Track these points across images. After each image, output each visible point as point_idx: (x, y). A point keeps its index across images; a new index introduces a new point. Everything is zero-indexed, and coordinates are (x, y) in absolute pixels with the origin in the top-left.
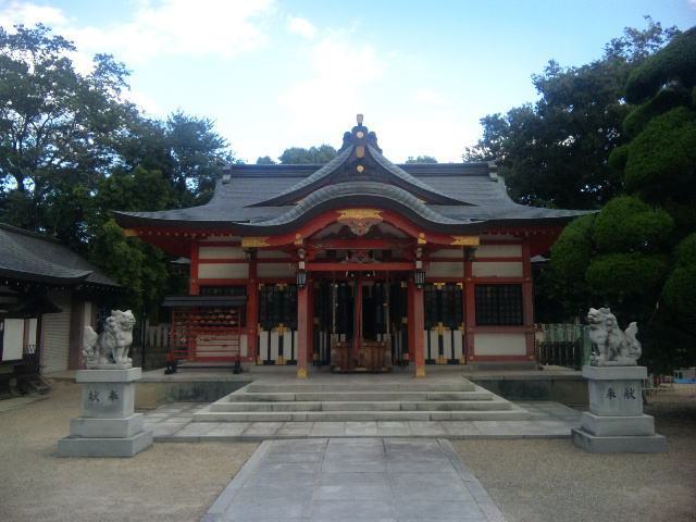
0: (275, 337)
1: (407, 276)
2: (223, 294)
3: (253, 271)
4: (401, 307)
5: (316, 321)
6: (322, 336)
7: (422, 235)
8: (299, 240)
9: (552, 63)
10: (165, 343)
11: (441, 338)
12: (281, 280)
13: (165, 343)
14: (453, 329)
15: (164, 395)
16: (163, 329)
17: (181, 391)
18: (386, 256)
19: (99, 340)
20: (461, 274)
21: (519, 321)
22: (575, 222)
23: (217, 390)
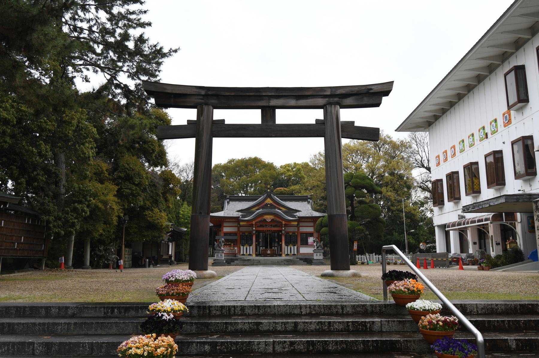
0: (245, 248)
1: (281, 231)
8: (254, 223)
9: (89, 82)
12: (247, 232)
14: (294, 246)
18: (276, 226)
20: (297, 230)
22: (397, 256)
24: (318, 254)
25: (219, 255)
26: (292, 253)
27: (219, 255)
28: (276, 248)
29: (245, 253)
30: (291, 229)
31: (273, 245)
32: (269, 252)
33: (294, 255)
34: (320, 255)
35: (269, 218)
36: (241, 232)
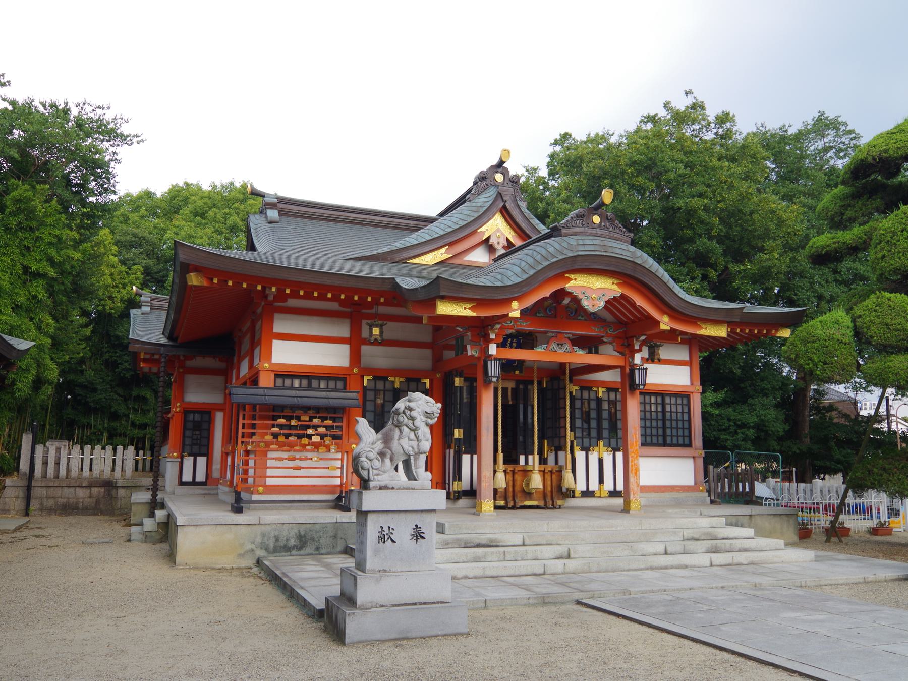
0: (594, 457)
2: (309, 387)
3: (355, 356)
10: (63, 472)
11: (601, 461)
12: (396, 372)
13: (63, 472)
14: (615, 450)
15: (249, 546)
16: (58, 450)
17: (277, 539)
19: (387, 441)
21: (687, 442)
23: (335, 537)
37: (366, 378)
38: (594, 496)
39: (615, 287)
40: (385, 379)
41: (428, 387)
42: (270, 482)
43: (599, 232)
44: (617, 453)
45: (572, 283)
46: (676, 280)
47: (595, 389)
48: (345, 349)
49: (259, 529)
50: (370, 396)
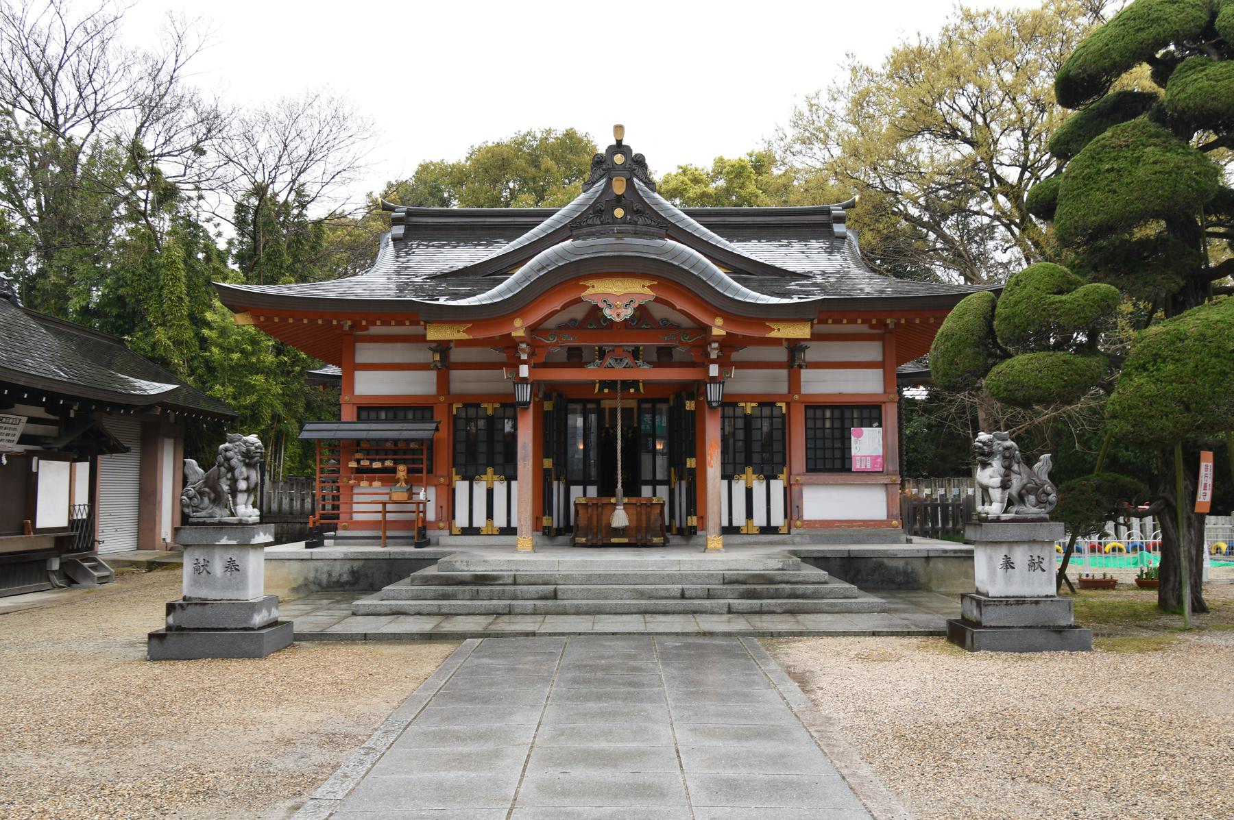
0: (480, 489)
1: (695, 389)
3: (443, 382)
4: (685, 442)
5: (548, 463)
6: (557, 487)
7: (719, 321)
8: (518, 328)
11: (749, 492)
12: (490, 398)
14: (769, 477)
18: (664, 357)
20: (783, 388)
24: (1020, 556)
25: (218, 567)
26: (759, 519)
27: (218, 567)
28: (663, 491)
29: (480, 520)
30: (752, 383)
31: (646, 474)
32: (620, 518)
33: (768, 530)
34: (1035, 564)
35: (618, 297)
36: (459, 397)
37: (455, 406)
38: (777, 533)
39: (647, 291)
40: (477, 406)
41: (784, 411)
42: (357, 517)
43: (624, 227)
44: (772, 482)
45: (590, 291)
46: (273, 281)
47: (743, 404)
48: (432, 375)
49: (312, 565)
50: (461, 424)
